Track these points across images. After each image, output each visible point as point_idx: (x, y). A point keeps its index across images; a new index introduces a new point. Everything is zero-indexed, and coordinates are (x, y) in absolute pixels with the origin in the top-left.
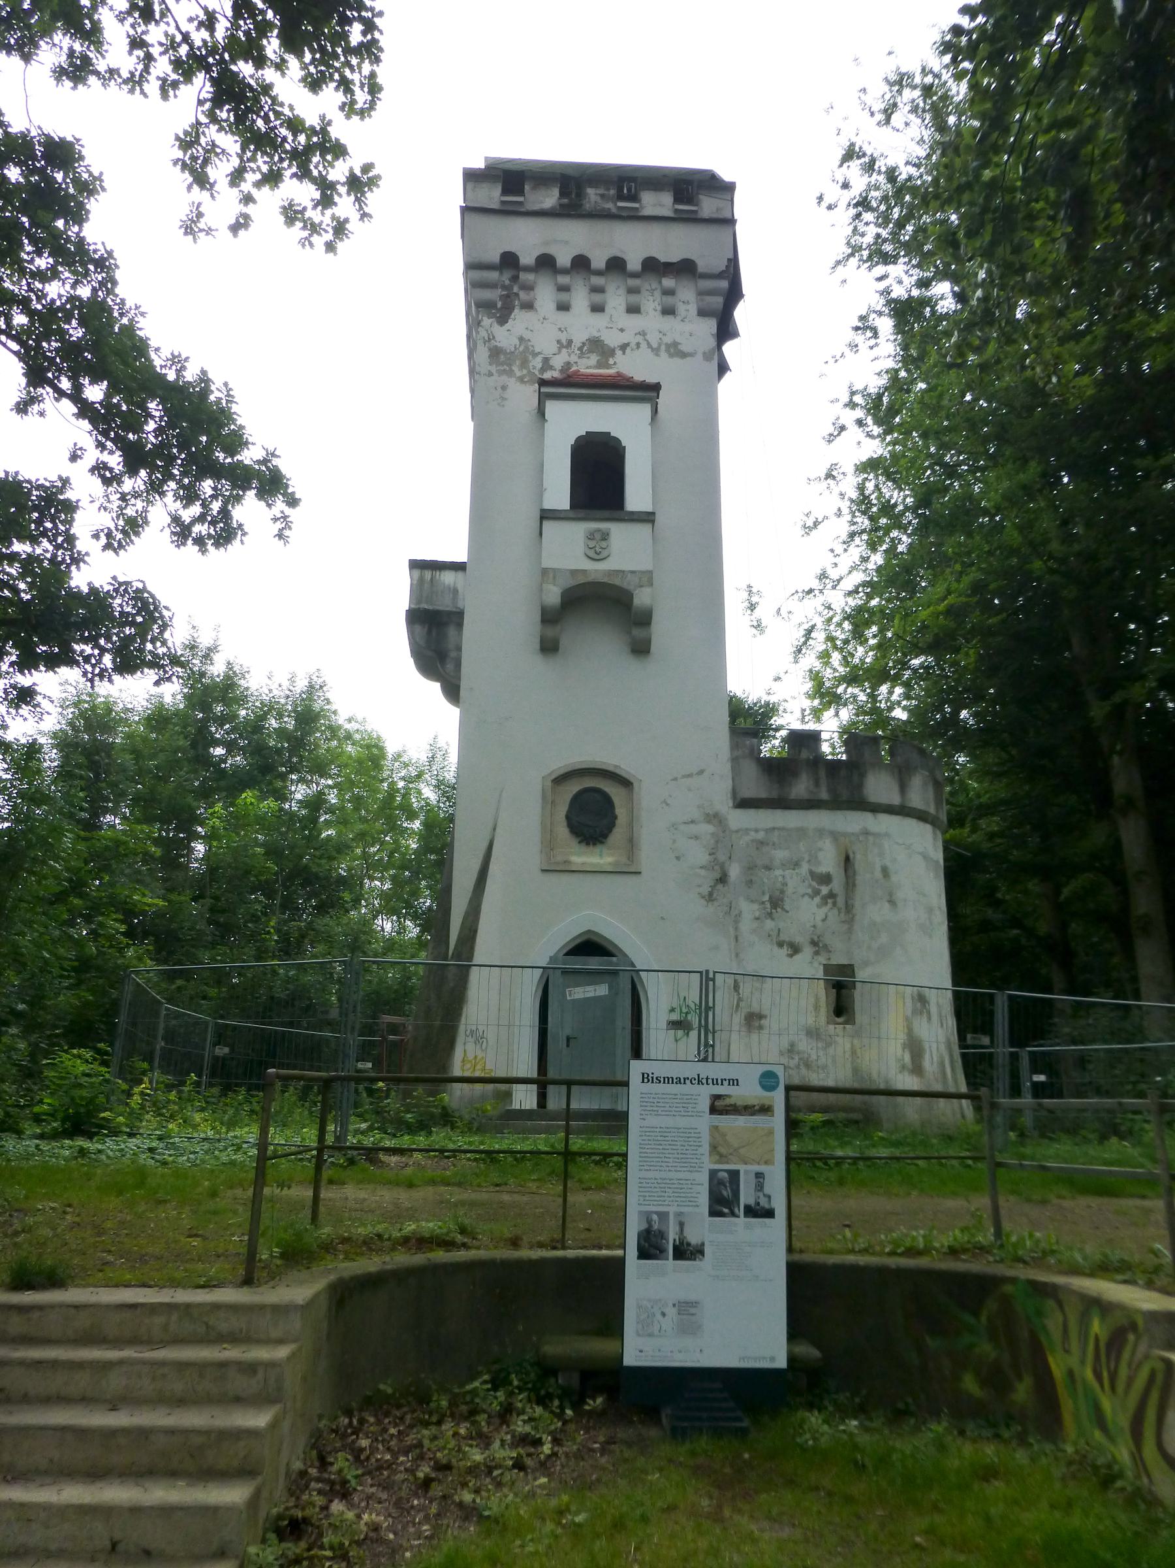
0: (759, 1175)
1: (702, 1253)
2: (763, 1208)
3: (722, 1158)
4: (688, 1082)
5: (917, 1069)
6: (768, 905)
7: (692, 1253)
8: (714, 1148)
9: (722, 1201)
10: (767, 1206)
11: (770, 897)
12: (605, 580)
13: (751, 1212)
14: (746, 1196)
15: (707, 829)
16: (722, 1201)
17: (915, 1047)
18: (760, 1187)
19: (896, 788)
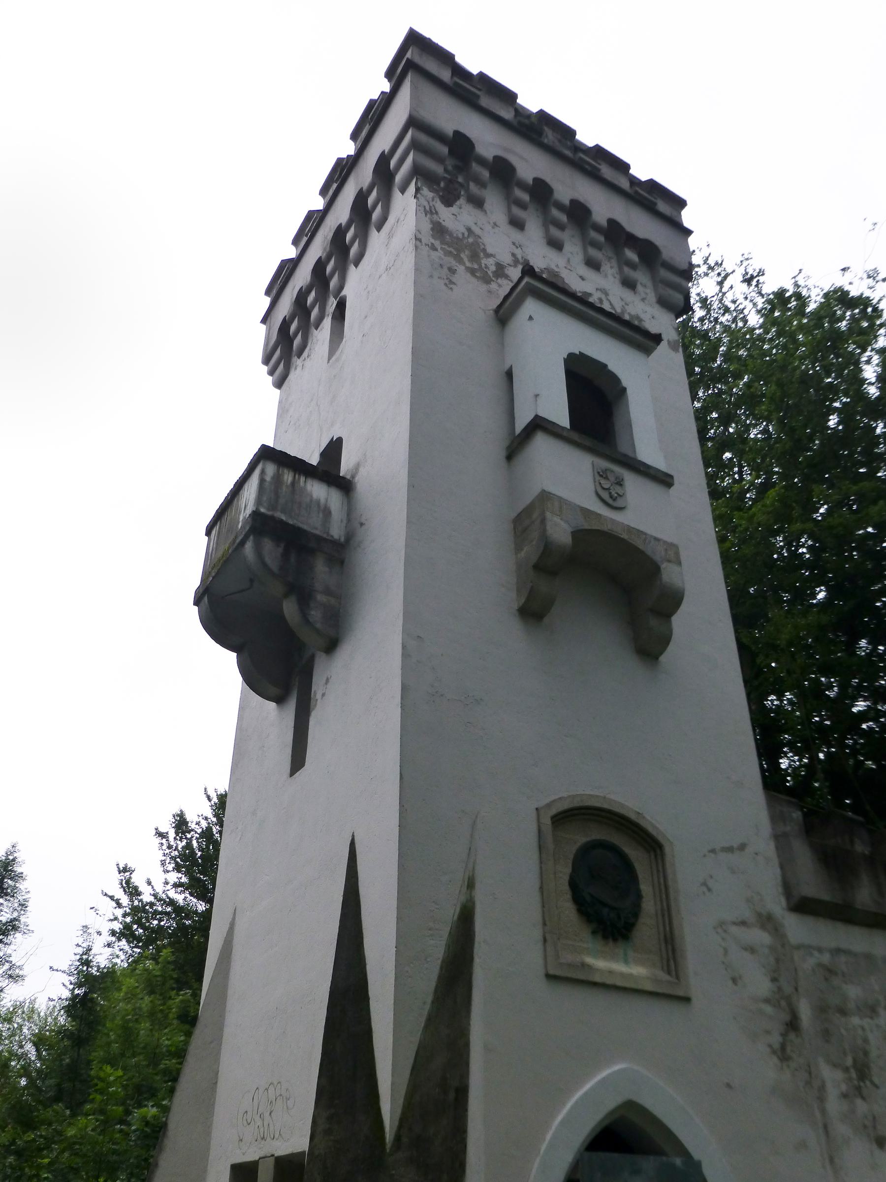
6: (854, 1075)
11: (855, 1060)
12: (625, 536)
15: (761, 937)
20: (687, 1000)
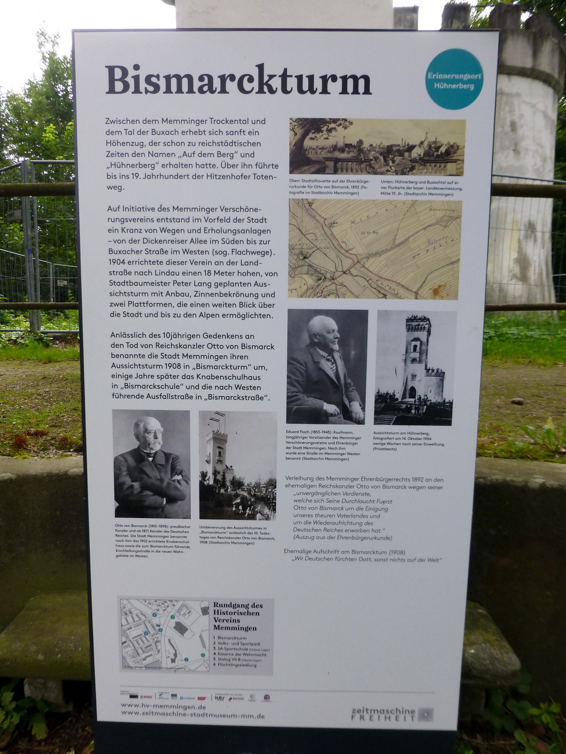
0: (417, 324)
1: (270, 502)
2: (423, 402)
3: (322, 282)
4: (231, 86)
5: (523, 278)
7: (245, 503)
8: (301, 258)
9: (321, 388)
10: (433, 398)
13: (390, 409)
14: (383, 373)
16: (321, 388)
17: (523, 262)
18: (417, 351)
19: (530, 52)
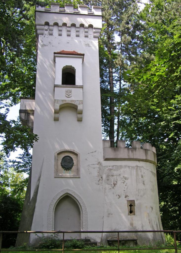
20: (80, 178)
